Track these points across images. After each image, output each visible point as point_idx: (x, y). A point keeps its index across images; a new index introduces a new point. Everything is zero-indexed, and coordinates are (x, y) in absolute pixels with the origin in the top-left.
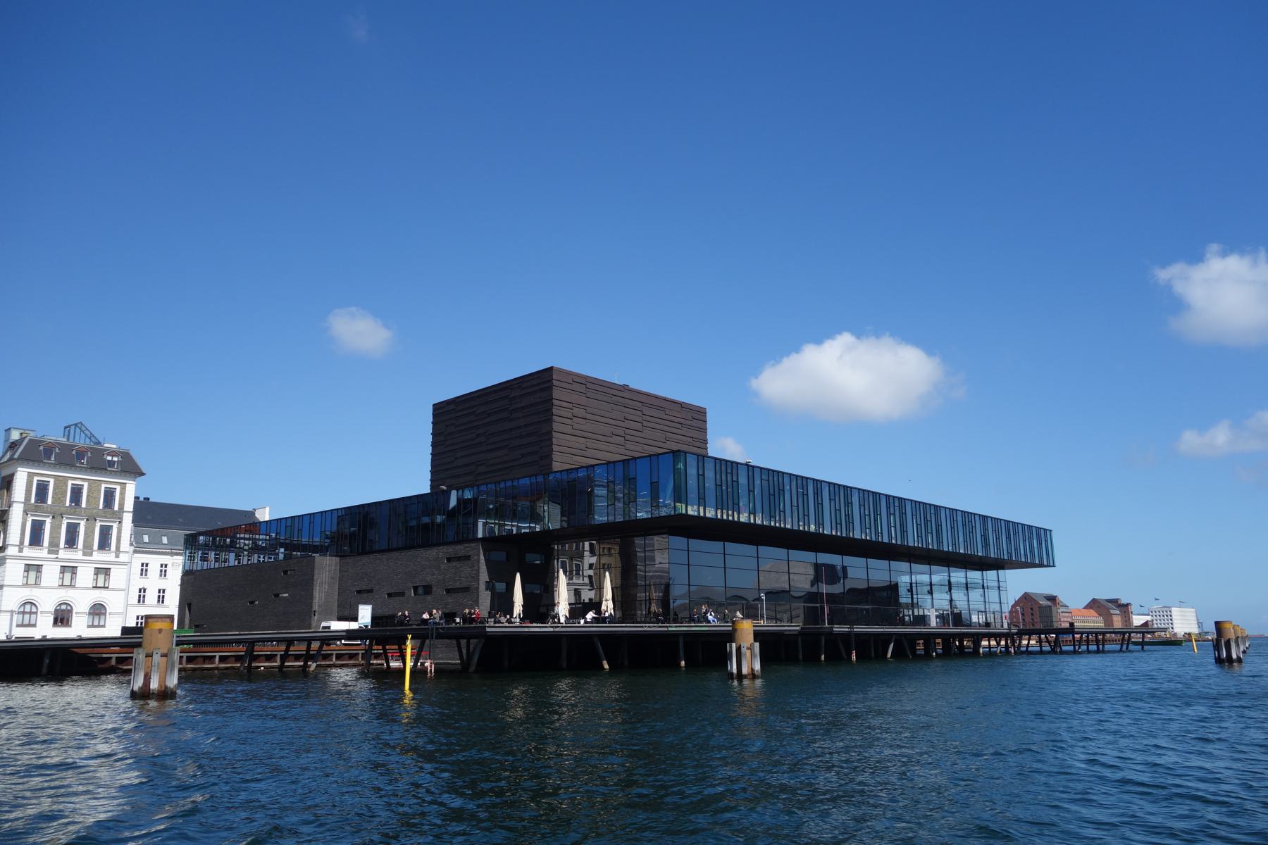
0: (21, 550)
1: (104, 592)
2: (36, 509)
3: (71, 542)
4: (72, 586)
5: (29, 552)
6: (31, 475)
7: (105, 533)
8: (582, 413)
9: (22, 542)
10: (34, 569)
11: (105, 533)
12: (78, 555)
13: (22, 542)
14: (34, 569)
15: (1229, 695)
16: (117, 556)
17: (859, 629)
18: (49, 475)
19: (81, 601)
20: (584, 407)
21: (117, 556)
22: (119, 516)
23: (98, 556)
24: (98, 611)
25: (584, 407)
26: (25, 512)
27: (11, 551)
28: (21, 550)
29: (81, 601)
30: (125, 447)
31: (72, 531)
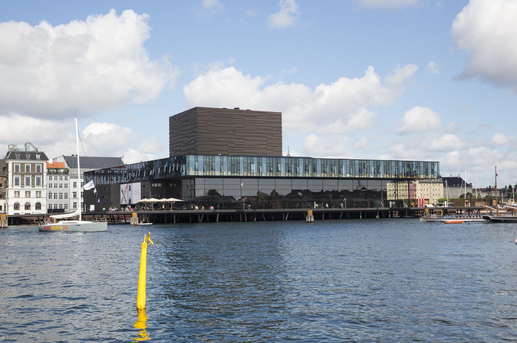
0: (13, 187)
1: (40, 199)
2: (16, 174)
3: (28, 184)
4: (29, 197)
5: (15, 187)
6: (13, 163)
7: (38, 180)
8: (272, 137)
9: (13, 184)
10: (17, 193)
11: (38, 180)
12: (41, 187)
13: (13, 184)
14: (17, 193)
15: (433, 183)
17: (258, 210)
18: (18, 162)
19: (33, 202)
20: (272, 134)
22: (42, 174)
23: (36, 187)
24: (38, 206)
25: (272, 134)
26: (13, 175)
27: (10, 187)
28: (13, 187)
29: (22, 202)
30: (42, 151)
31: (28, 180)
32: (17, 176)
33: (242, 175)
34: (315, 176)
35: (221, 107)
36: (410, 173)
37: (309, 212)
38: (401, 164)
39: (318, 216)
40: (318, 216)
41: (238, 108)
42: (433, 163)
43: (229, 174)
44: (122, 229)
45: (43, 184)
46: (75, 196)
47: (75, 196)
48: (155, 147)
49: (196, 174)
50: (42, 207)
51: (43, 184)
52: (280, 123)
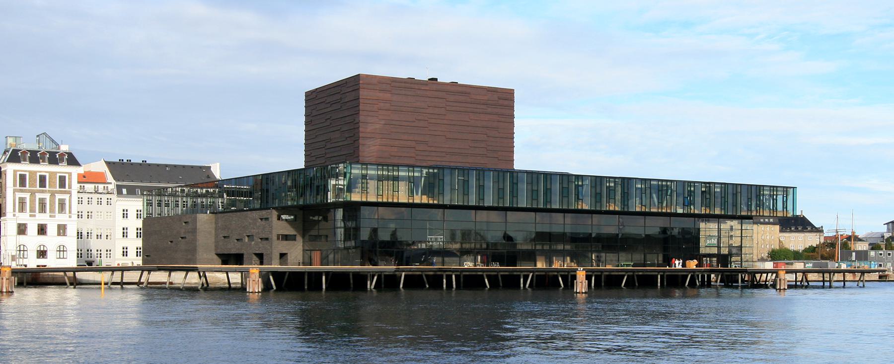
4: (64, 235)
7: (62, 204)
16: (70, 217)
21: (70, 217)
32: (22, 195)
33: (447, 202)
34: (580, 207)
35: (423, 75)
36: (743, 202)
37: (251, 271)
38: (556, 187)
39: (605, 283)
40: (605, 283)
41: (436, 79)
42: (786, 189)
43: (425, 200)
44: (632, 307)
45: (70, 212)
46: (125, 235)
47: (125, 235)
48: (284, 149)
49: (364, 200)
50: (49, 253)
51: (70, 212)
52: (512, 108)
